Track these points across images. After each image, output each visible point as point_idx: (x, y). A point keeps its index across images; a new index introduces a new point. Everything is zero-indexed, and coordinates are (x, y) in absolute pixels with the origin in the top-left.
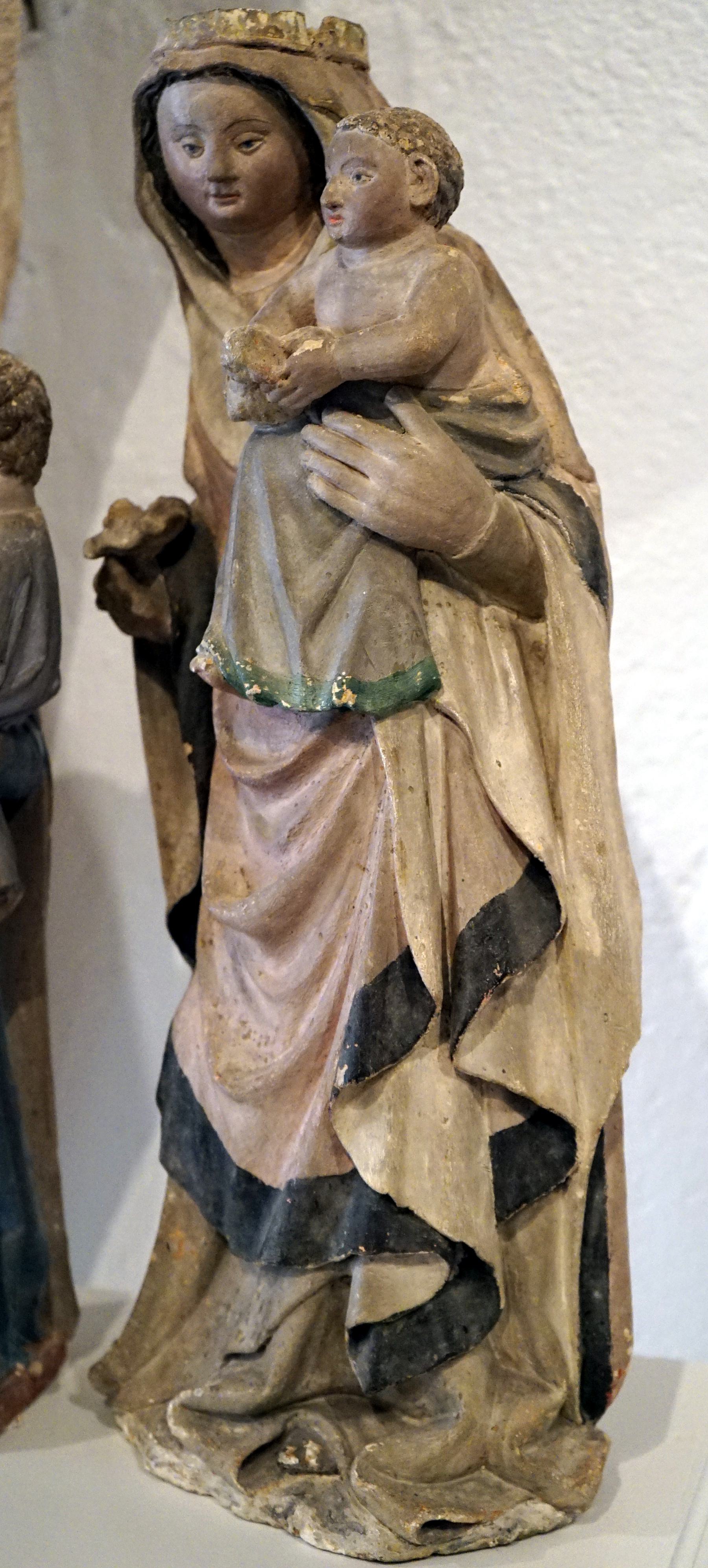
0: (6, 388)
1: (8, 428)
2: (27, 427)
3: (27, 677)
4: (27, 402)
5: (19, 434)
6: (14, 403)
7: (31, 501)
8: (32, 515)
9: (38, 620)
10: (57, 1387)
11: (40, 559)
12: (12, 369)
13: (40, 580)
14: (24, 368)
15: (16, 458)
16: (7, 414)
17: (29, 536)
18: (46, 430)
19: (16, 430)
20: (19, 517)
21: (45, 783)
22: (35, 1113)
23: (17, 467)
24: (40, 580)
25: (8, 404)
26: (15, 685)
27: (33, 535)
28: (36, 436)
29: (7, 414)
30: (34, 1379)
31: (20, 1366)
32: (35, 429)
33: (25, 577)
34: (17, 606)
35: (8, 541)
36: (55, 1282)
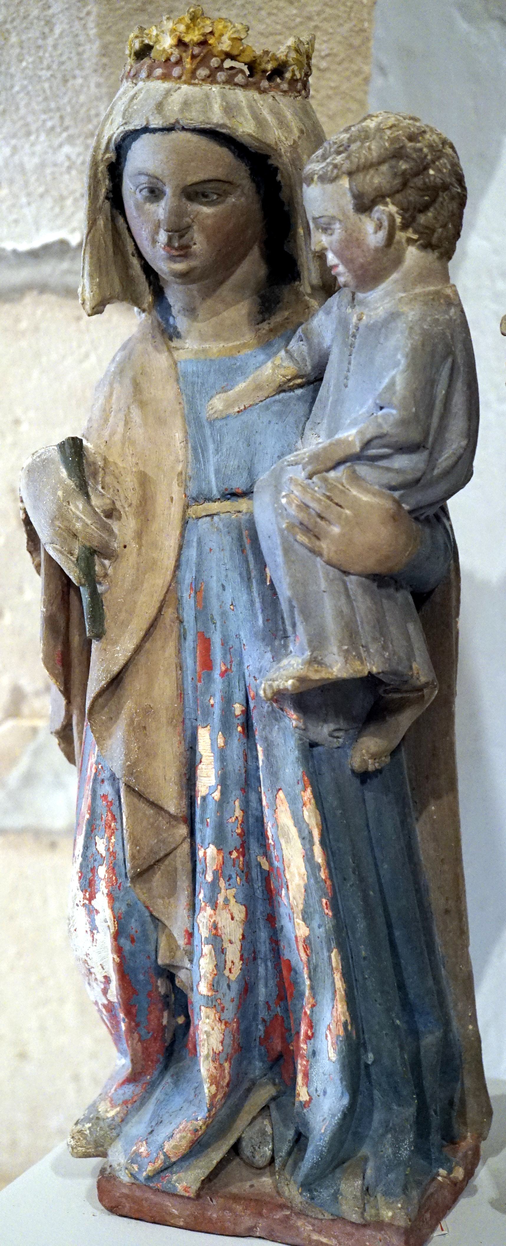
0: (423, 156)
1: (426, 198)
2: (444, 197)
3: (450, 462)
4: (445, 171)
5: (437, 205)
6: (431, 172)
7: (445, 277)
8: (449, 291)
9: (459, 400)
10: (475, 1191)
11: (460, 337)
12: (427, 136)
13: (460, 361)
14: (438, 134)
15: (433, 231)
16: (425, 183)
17: (448, 314)
18: (462, 200)
19: (433, 201)
20: (437, 293)
21: (453, 576)
22: (447, 912)
23: (434, 240)
24: (460, 361)
25: (425, 172)
26: (436, 472)
27: (452, 311)
28: (454, 205)
29: (425, 183)
30: (455, 1183)
31: (442, 1171)
32: (452, 198)
33: (445, 358)
34: (439, 386)
35: (429, 319)
36: (468, 1082)
